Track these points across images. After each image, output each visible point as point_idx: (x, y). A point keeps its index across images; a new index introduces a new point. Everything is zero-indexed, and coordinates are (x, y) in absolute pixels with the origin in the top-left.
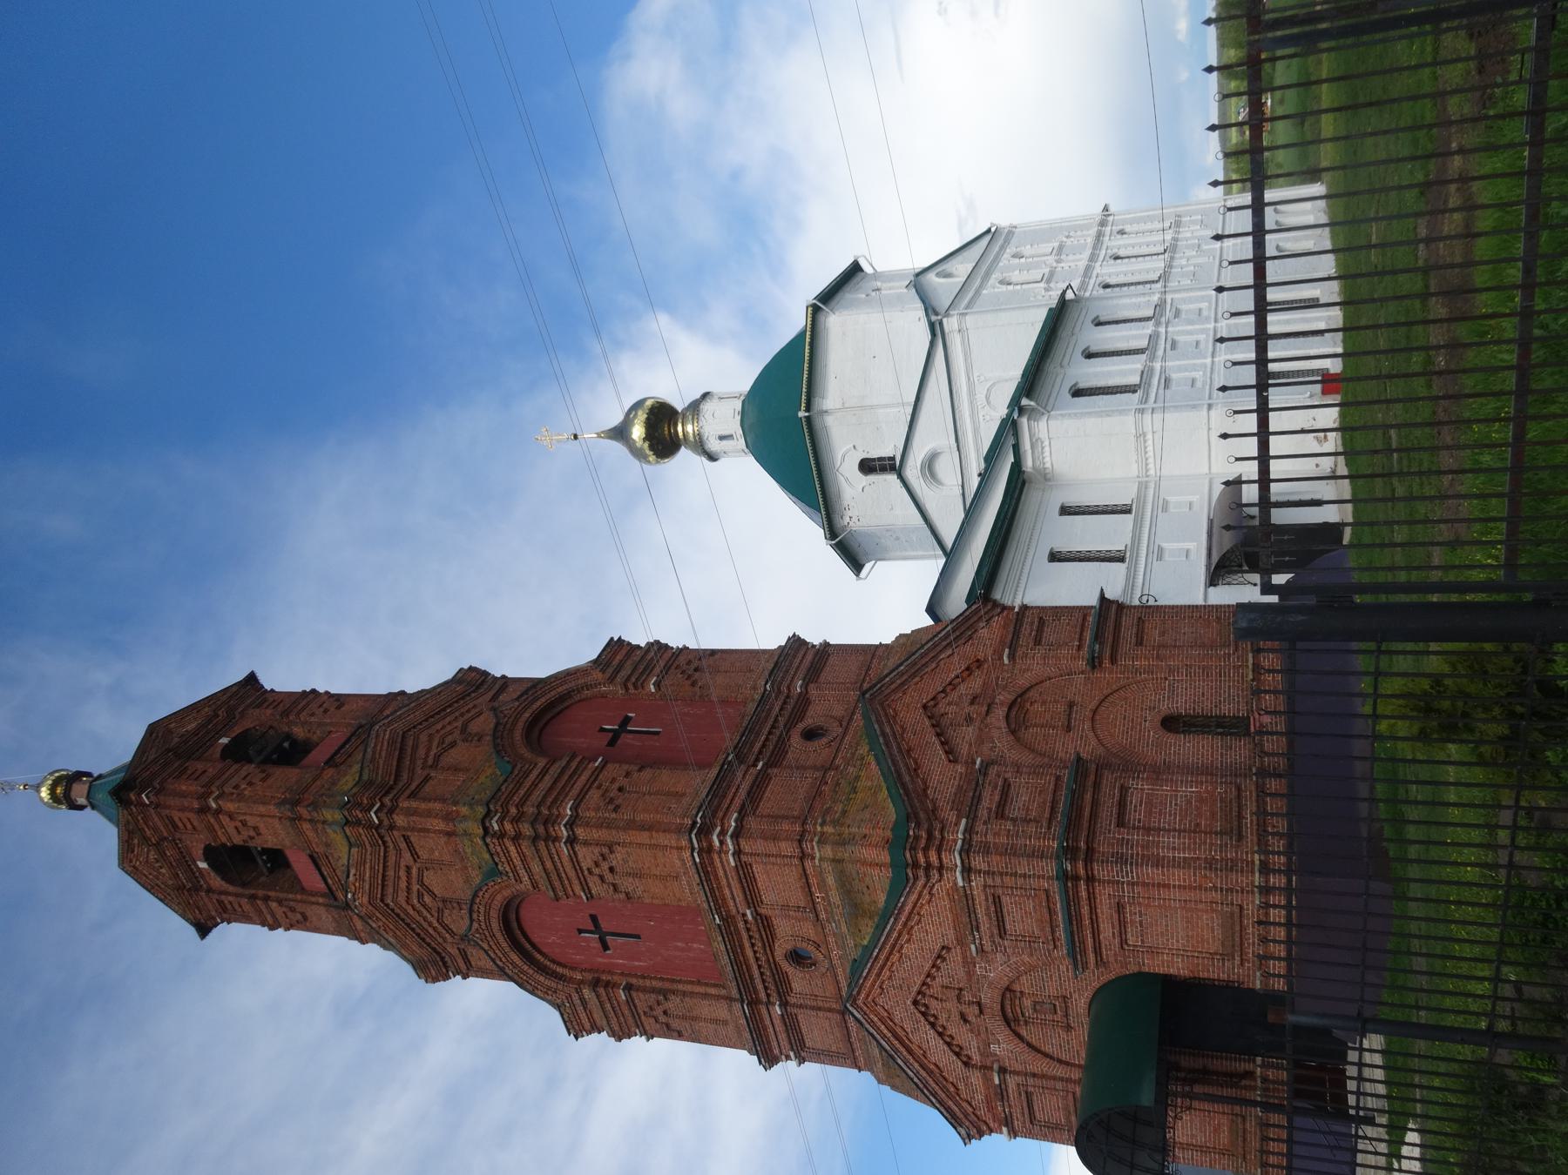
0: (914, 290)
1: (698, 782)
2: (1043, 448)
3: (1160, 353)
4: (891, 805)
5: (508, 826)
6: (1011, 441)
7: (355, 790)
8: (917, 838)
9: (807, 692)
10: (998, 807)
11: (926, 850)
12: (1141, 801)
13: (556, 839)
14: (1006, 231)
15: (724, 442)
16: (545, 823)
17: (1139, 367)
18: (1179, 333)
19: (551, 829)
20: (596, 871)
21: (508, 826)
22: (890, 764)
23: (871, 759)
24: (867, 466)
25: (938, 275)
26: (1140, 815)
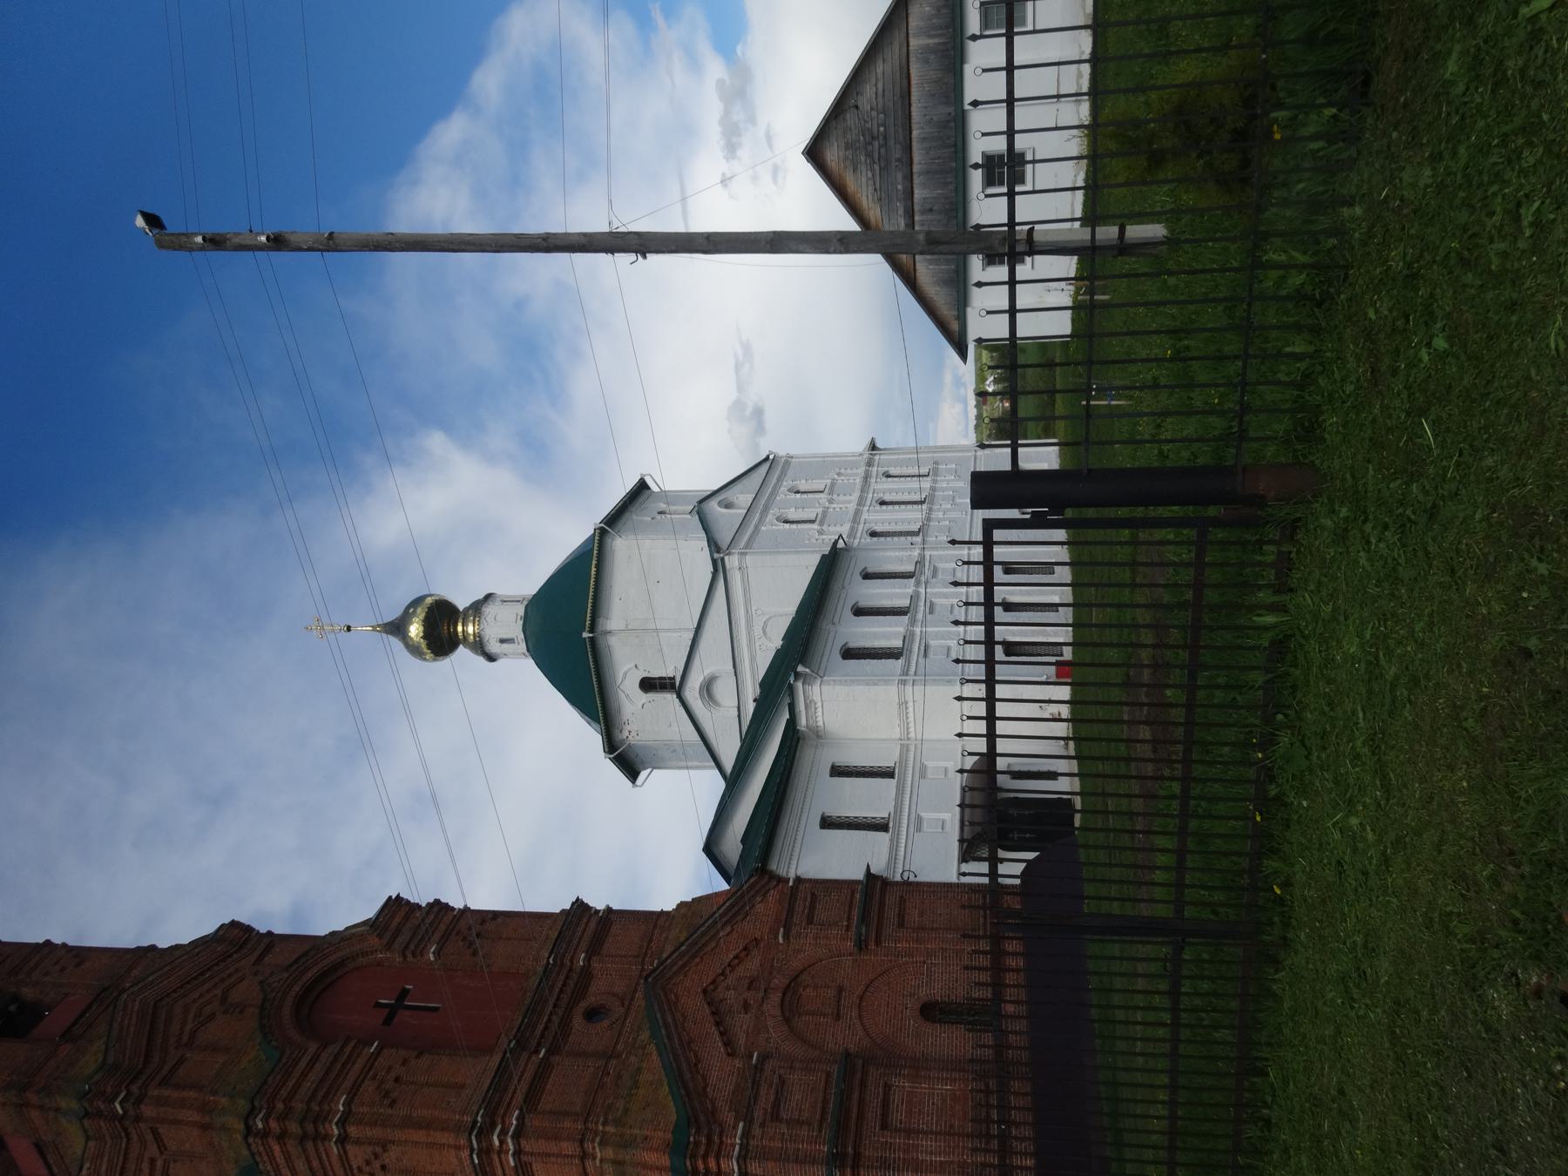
0: (697, 517)
1: (476, 1072)
2: (816, 709)
3: (920, 616)
4: (672, 1103)
5: (273, 1124)
6: (787, 700)
7: (97, 1077)
8: (697, 1144)
9: (590, 965)
10: (773, 1108)
11: (705, 1157)
12: (903, 1099)
13: (327, 1137)
14: (783, 460)
15: (505, 646)
16: (315, 1122)
17: (902, 630)
18: (936, 594)
19: (321, 1127)
20: (367, 1169)
21: (273, 1124)
22: (672, 1060)
23: (652, 1048)
24: (648, 685)
25: (720, 504)
26: (901, 1115)
